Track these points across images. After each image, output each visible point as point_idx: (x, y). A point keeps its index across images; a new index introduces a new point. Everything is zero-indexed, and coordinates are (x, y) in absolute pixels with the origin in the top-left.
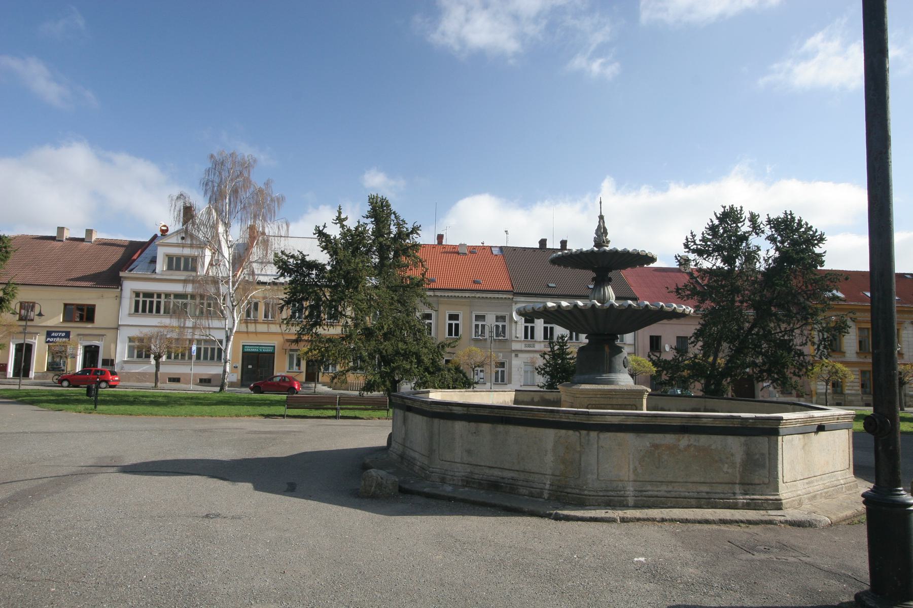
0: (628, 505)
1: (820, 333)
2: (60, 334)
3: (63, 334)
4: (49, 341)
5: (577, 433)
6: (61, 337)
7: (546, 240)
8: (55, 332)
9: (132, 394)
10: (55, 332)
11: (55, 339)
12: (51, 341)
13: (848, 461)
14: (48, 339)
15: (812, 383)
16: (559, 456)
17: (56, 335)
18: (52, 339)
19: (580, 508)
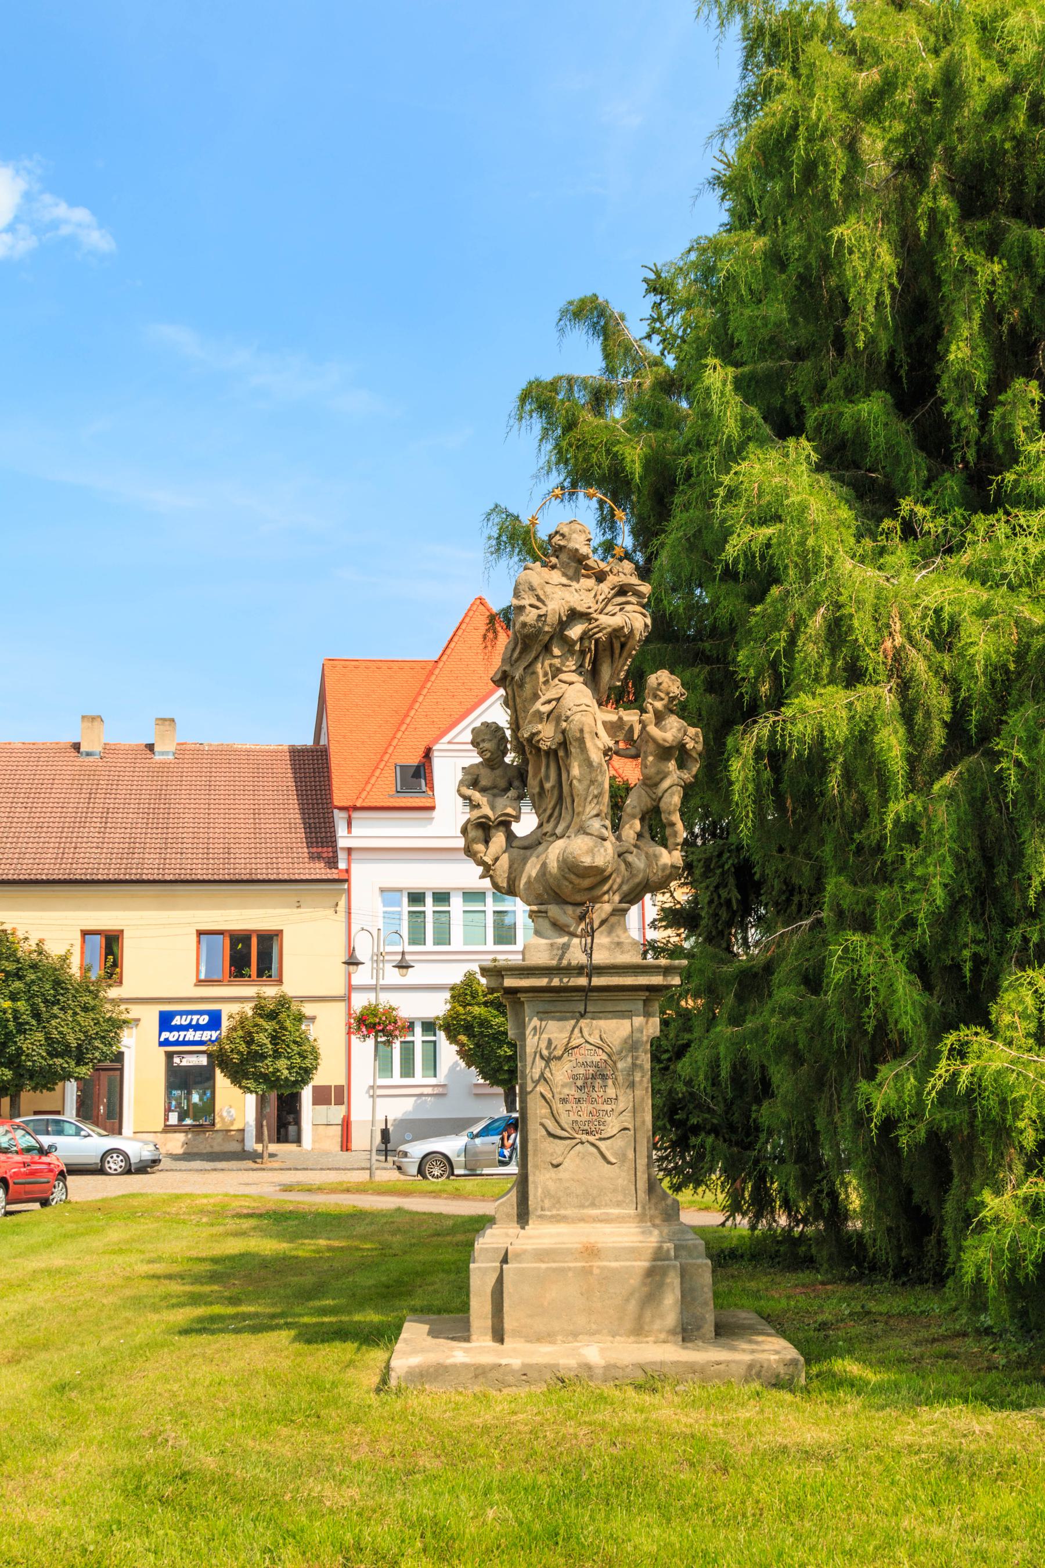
0: (298, 755)
1: (563, 676)
2: (195, 1017)
3: (177, 1021)
4: (167, 1040)
5: (340, 1122)
6: (198, 1027)
7: (413, 777)
8: (181, 1013)
9: (235, 1204)
10: (181, 1013)
11: (182, 1034)
12: (171, 1039)
13: (214, 1175)
14: (165, 1035)
15: (692, 731)
16: (942, 1454)
17: (183, 1021)
18: (176, 1034)
19: (660, 1102)
